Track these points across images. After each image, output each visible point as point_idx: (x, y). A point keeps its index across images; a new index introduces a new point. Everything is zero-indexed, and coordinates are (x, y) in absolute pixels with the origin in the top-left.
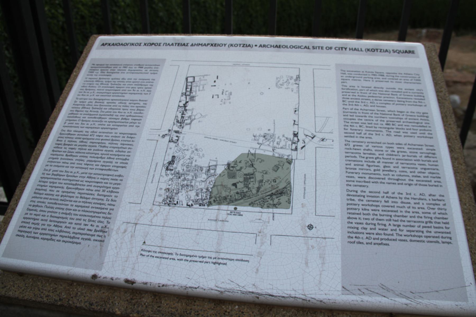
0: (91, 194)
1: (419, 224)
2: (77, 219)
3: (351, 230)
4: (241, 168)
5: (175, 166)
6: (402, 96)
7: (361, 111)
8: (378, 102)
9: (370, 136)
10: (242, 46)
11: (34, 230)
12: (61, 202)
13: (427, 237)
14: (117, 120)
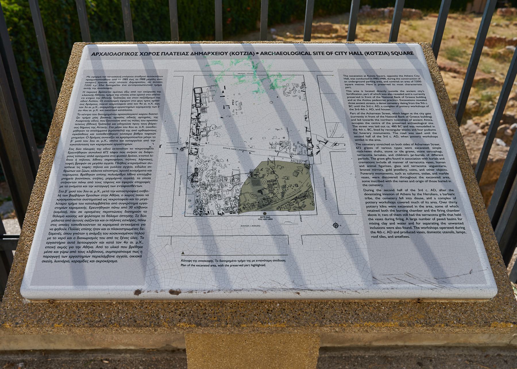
0: (118, 212)
1: (433, 217)
2: (108, 238)
3: (373, 226)
4: (264, 175)
5: (199, 177)
6: (405, 99)
7: (368, 115)
8: (383, 105)
9: (379, 138)
10: (243, 53)
11: (62, 254)
12: (87, 223)
13: (442, 228)
14: (130, 136)
